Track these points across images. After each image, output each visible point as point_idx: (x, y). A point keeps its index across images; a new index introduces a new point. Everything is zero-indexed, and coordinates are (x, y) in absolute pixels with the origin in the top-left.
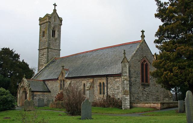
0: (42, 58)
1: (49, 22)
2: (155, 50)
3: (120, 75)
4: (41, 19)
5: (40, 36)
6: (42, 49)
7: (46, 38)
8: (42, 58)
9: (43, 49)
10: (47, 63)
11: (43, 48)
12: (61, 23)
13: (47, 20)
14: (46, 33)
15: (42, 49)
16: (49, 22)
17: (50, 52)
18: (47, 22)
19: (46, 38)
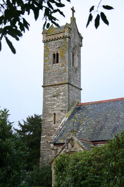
0: (54, 100)
1: (69, 37)
2: (4, 16)
3: (51, 37)
4: (42, 33)
5: (45, 61)
6: (52, 86)
7: (62, 66)
8: (54, 100)
9: (55, 85)
10: (68, 110)
11: (56, 82)
12: (81, 43)
13: (66, 34)
14: (64, 58)
15: (52, 86)
16: (69, 37)
17: (71, 92)
18: (64, 38)
19: (62, 66)
